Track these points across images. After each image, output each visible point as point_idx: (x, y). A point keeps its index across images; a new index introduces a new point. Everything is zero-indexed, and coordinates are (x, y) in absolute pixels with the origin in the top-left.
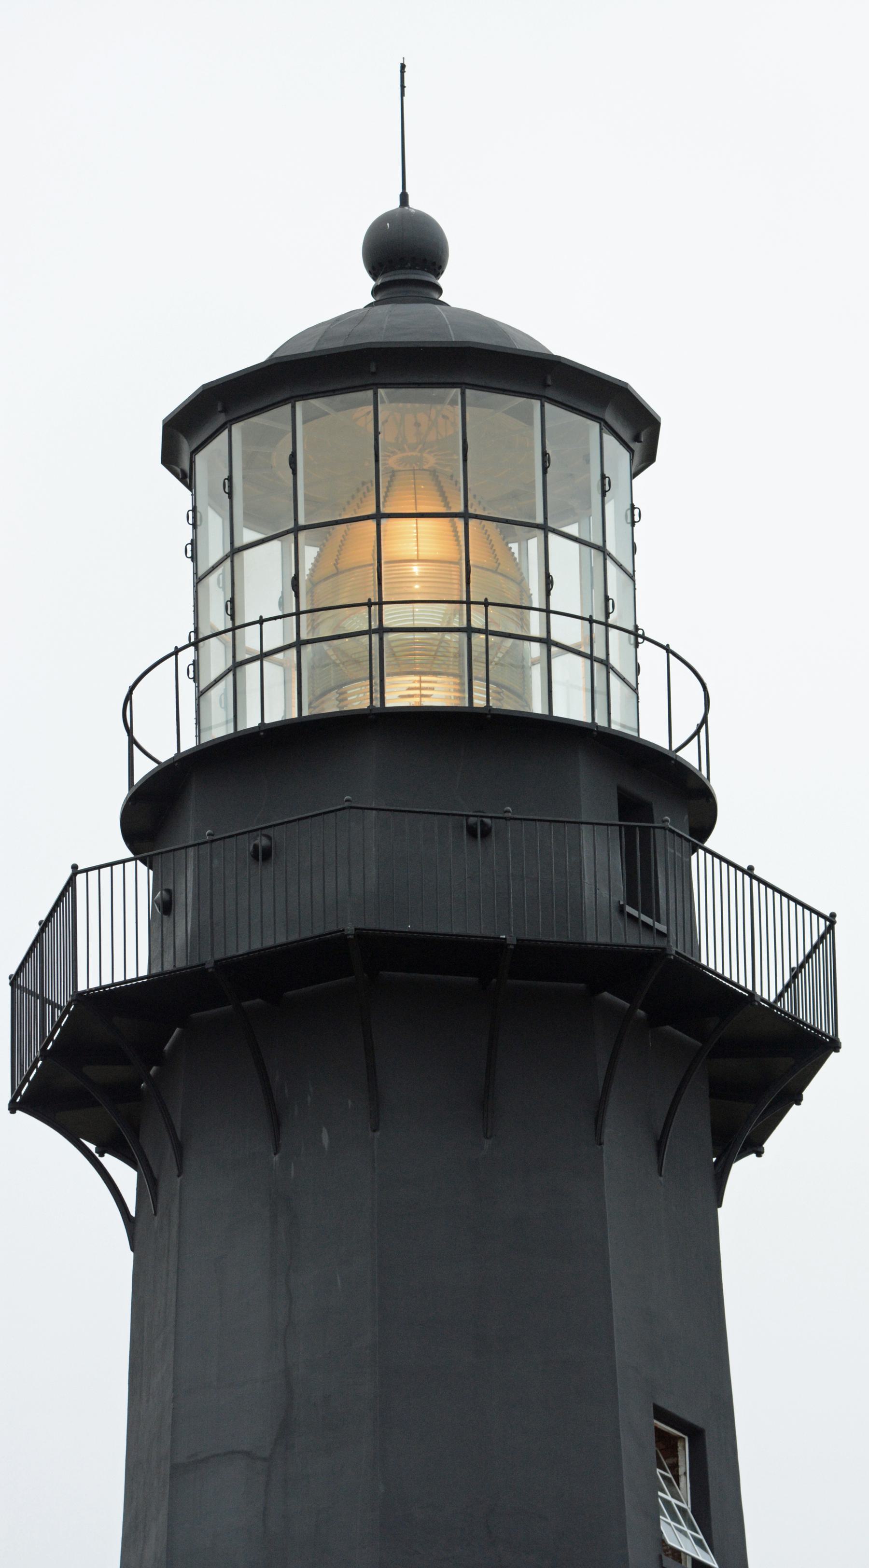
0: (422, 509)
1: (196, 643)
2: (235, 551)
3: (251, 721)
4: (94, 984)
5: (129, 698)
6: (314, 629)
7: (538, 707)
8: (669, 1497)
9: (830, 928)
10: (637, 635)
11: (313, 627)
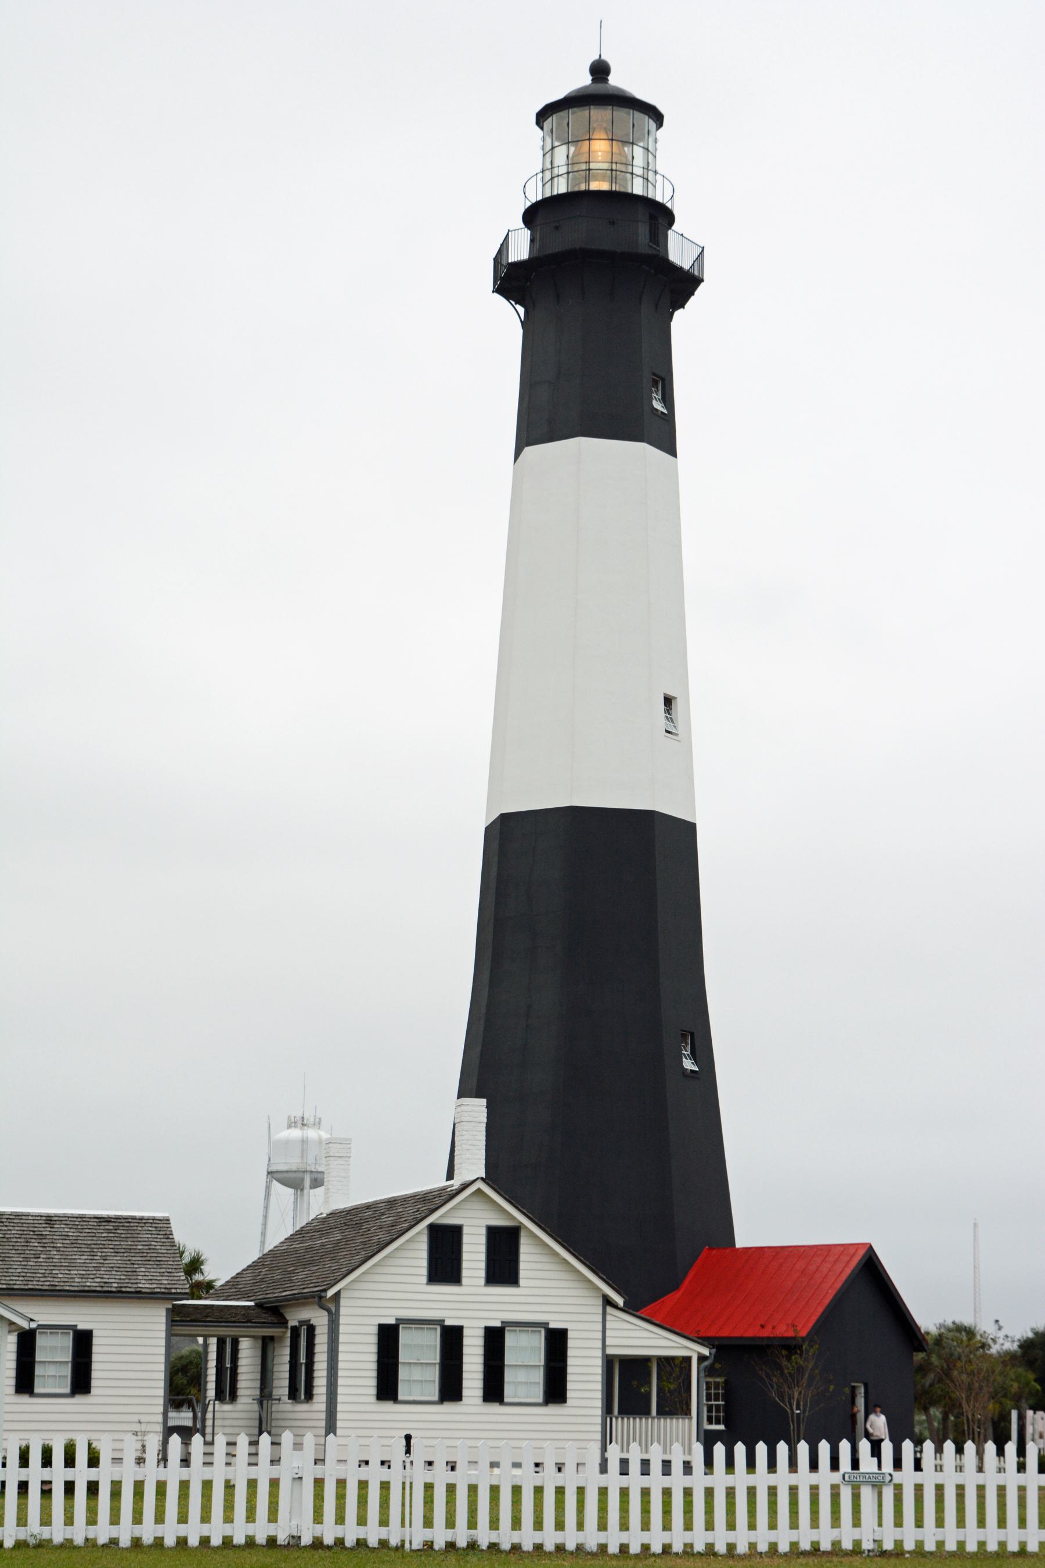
0: (602, 138)
1: (543, 171)
2: (553, 148)
3: (555, 193)
4: (513, 261)
5: (525, 186)
6: (573, 169)
7: (630, 191)
8: (655, 395)
9: (703, 251)
10: (656, 172)
11: (573, 168)
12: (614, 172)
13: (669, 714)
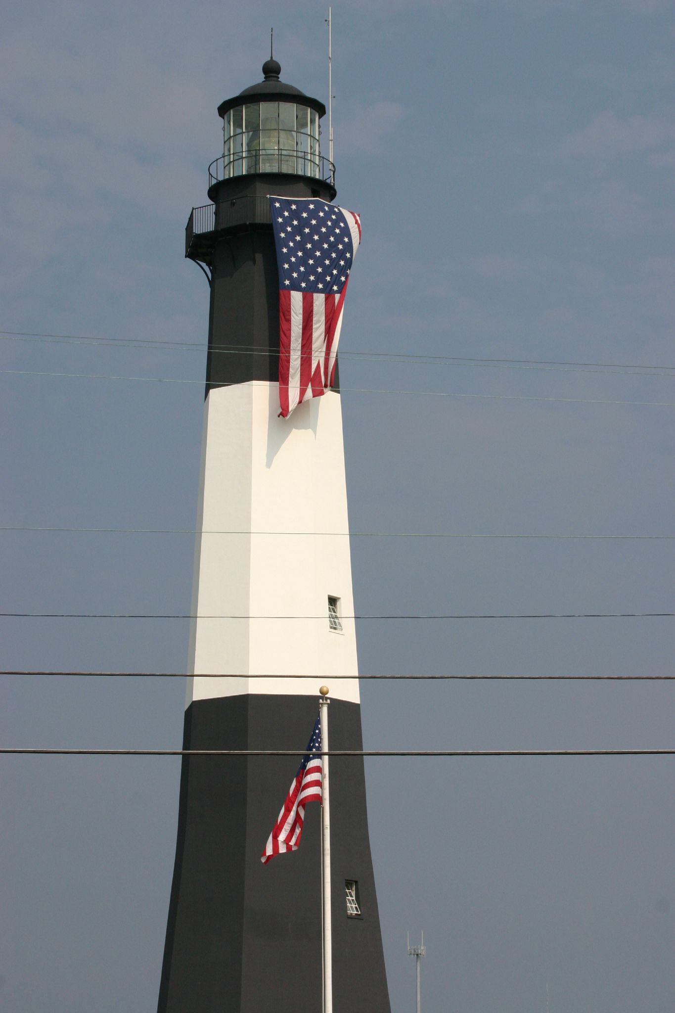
12: (280, 151)
13: (335, 612)
